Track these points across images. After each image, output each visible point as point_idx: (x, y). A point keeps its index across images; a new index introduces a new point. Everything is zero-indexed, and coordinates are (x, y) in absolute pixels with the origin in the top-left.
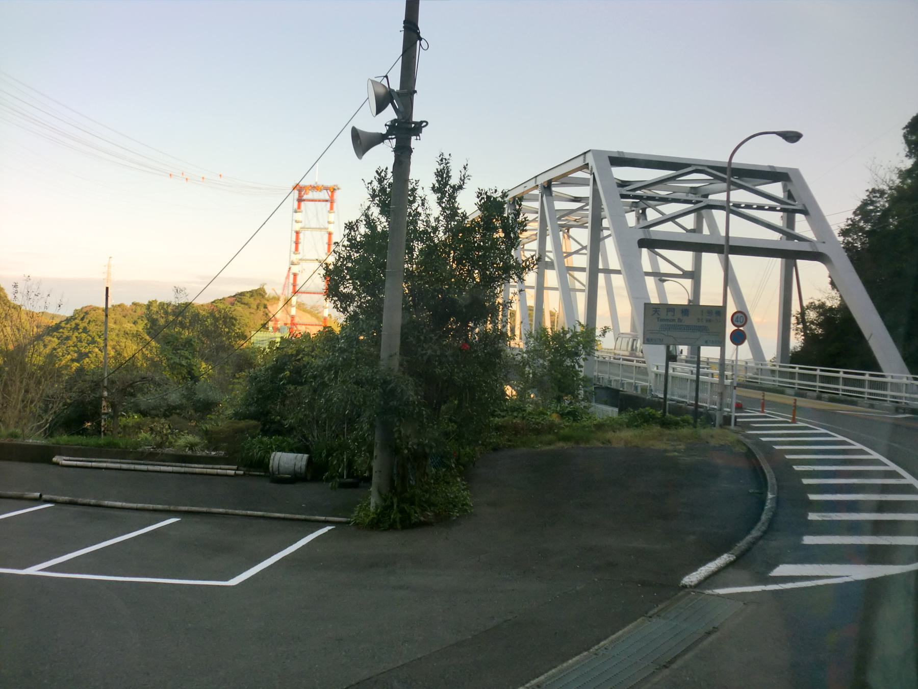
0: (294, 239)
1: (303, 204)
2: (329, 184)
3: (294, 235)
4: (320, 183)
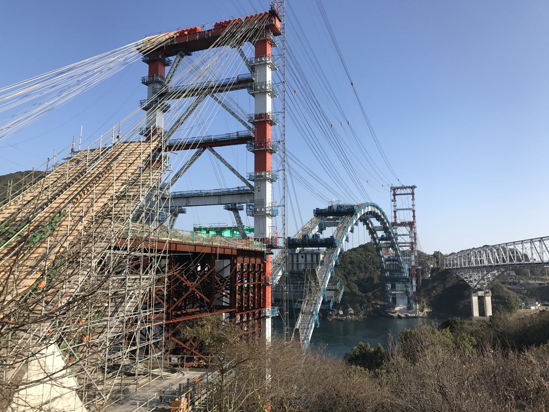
0: (393, 215)
2: (411, 185)
4: (405, 185)
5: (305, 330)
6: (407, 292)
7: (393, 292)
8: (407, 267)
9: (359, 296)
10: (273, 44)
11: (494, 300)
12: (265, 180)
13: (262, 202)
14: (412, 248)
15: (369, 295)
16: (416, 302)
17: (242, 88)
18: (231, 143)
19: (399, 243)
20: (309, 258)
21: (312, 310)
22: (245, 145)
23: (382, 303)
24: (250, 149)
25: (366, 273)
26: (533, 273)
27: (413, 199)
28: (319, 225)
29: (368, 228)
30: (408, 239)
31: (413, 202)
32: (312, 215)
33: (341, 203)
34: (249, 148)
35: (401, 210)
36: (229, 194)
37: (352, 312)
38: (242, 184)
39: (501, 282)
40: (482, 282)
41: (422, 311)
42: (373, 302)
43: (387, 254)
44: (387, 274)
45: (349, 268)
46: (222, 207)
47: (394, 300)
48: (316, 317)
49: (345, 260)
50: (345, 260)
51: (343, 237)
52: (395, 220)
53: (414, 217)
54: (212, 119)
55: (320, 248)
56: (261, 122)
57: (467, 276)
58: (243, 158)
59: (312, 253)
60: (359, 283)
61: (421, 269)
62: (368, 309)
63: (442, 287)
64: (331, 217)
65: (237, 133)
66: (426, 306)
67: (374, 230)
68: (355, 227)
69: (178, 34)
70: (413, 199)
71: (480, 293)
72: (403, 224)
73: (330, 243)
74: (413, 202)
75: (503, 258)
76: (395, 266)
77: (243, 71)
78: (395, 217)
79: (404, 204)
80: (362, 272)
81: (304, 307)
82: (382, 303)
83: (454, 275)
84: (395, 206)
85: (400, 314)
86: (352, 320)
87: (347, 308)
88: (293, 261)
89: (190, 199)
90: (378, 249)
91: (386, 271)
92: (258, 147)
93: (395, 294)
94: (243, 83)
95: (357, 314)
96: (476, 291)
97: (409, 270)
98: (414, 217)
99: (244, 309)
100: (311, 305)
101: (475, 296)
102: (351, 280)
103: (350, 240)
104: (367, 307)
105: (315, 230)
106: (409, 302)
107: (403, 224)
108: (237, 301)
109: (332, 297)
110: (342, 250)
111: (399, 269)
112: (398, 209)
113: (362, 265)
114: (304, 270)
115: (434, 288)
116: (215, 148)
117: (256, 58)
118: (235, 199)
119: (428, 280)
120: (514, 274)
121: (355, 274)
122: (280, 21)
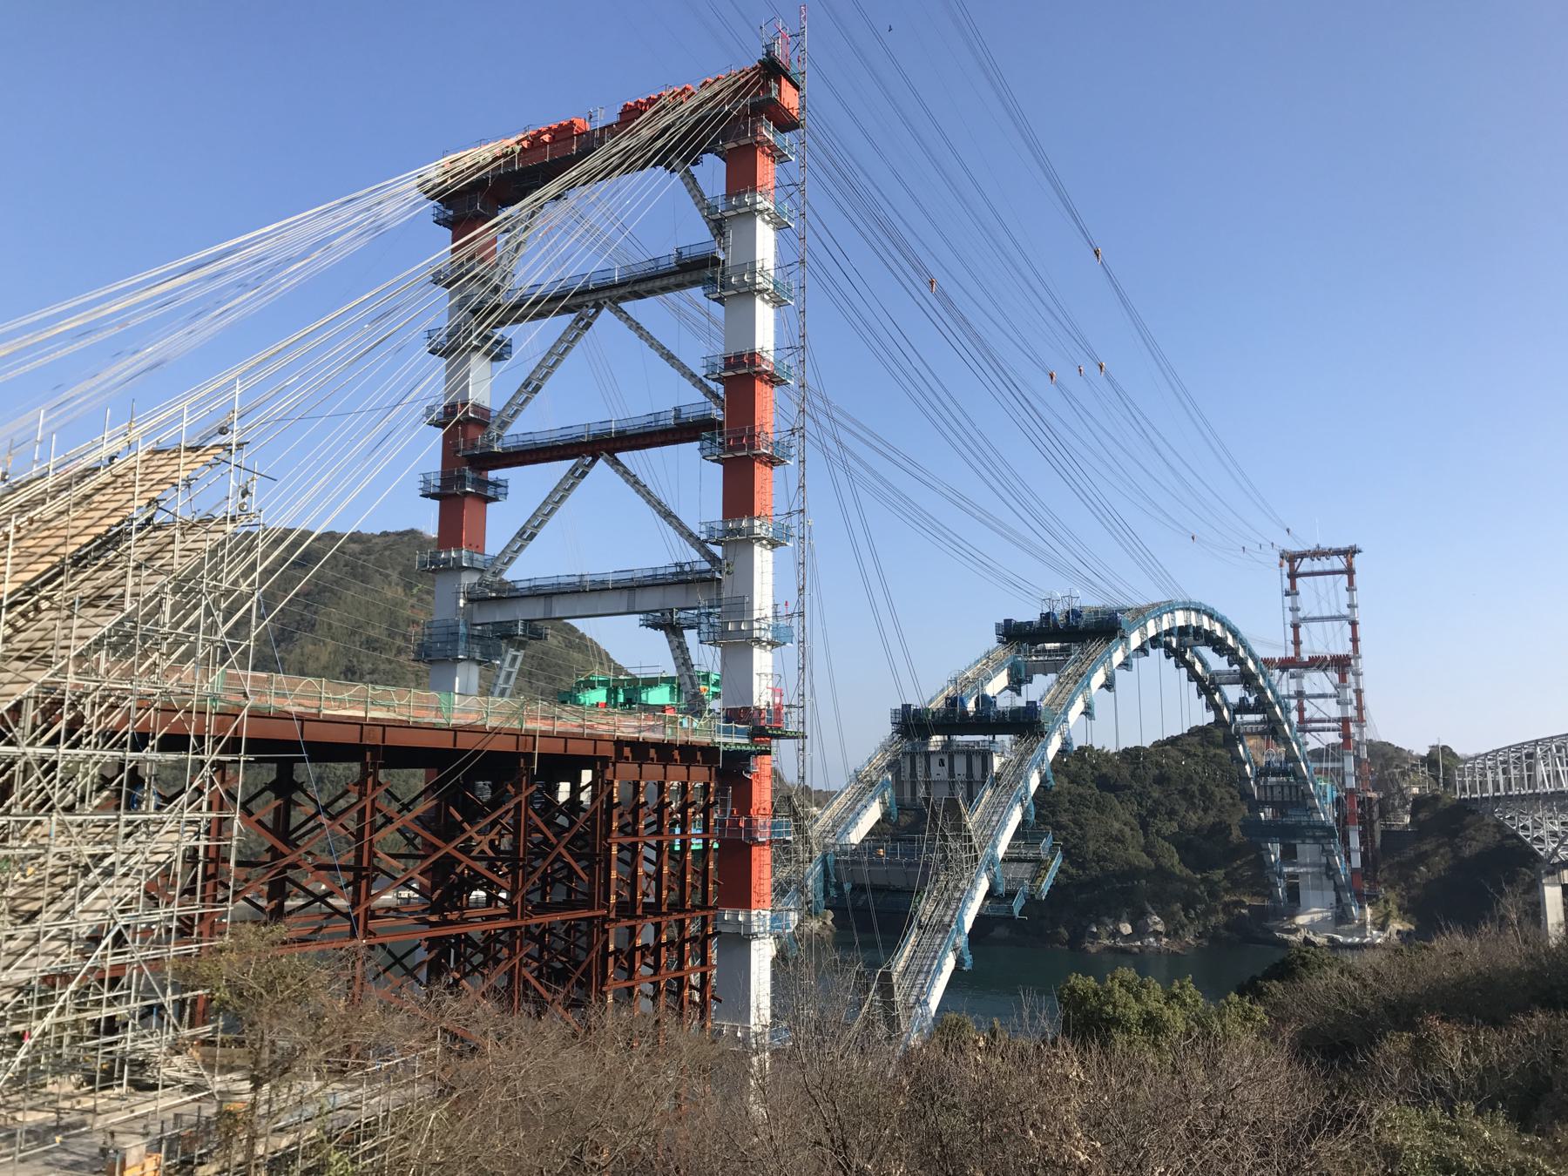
0: (1290, 636)
2: (1344, 545)
4: (1325, 545)
5: (922, 976)
6: (1330, 871)
7: (1286, 870)
8: (1331, 793)
10: (778, 156)
12: (749, 540)
13: (742, 606)
15: (1215, 878)
16: (1361, 898)
18: (670, 437)
19: (1311, 721)
20: (960, 765)
21: (947, 919)
22: (697, 444)
23: (1256, 902)
24: (712, 454)
25: (1205, 810)
27: (1351, 587)
28: (1010, 669)
29: (1193, 676)
30: (1332, 709)
31: (1352, 598)
32: (991, 641)
33: (1076, 605)
34: (707, 452)
35: (1314, 619)
36: (654, 582)
37: (1160, 928)
41: (1383, 928)
42: (1227, 898)
43: (1253, 752)
44: (1265, 814)
45: (1156, 795)
46: (635, 619)
47: (1293, 893)
48: (962, 941)
49: (1140, 772)
50: (1140, 772)
51: (1072, 702)
54: (618, 374)
55: (998, 738)
56: (741, 376)
57: (1529, 823)
58: (691, 479)
59: (969, 753)
60: (1185, 845)
61: (1379, 801)
62: (1213, 920)
63: (1450, 855)
64: (1049, 646)
66: (1395, 913)
67: (1212, 681)
68: (1121, 675)
69: (525, 144)
70: (1351, 587)
72: (1317, 663)
73: (1027, 724)
74: (1352, 598)
76: (1286, 791)
77: (695, 235)
78: (1297, 642)
79: (1324, 605)
80: (1192, 806)
81: (926, 908)
83: (1488, 819)
84: (1294, 609)
85: (1311, 936)
88: (913, 774)
89: (554, 598)
91: (1262, 804)
92: (731, 449)
93: (1294, 876)
94: (695, 270)
95: (1176, 932)
97: (1338, 803)
99: (639, 912)
100: (947, 905)
101: (1553, 884)
102: (1158, 832)
106: (1339, 900)
107: (1317, 663)
108: (613, 888)
110: (1066, 743)
111: (1299, 798)
112: (1305, 619)
113: (1195, 788)
115: (1422, 858)
116: (622, 456)
117: (728, 196)
119: (1402, 833)
121: (1171, 814)
122: (797, 87)
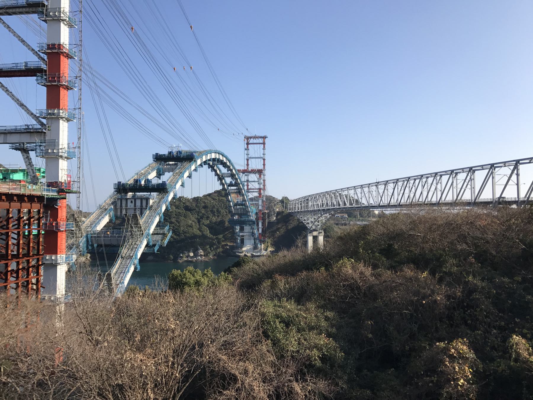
0: (246, 163)
1: (249, 145)
2: (263, 135)
3: (246, 161)
4: (258, 135)
5: (122, 274)
6: (253, 234)
9: (210, 238)
11: (326, 239)
12: (58, 118)
13: (55, 143)
14: (260, 194)
16: (262, 242)
17: (34, 12)
20: (138, 203)
21: (131, 255)
22: (35, 78)
23: (231, 244)
25: (218, 216)
26: (361, 216)
27: (264, 148)
29: (217, 174)
30: (256, 186)
32: (151, 160)
33: (180, 149)
35: (253, 158)
37: (202, 254)
38: (32, 122)
39: (335, 224)
40: (316, 223)
41: (266, 250)
42: (223, 243)
43: (233, 198)
44: (236, 217)
45: (203, 212)
47: (242, 241)
48: (137, 261)
49: (199, 205)
52: (248, 168)
53: (264, 165)
55: (152, 193)
56: (54, 53)
57: (306, 219)
58: (33, 92)
59: (141, 199)
60: (211, 227)
64: (171, 163)
65: (26, 63)
66: (270, 246)
67: (222, 176)
70: (264, 148)
71: (315, 233)
72: (253, 171)
73: (162, 189)
75: (344, 201)
78: (248, 165)
80: (214, 215)
82: (231, 244)
84: (248, 154)
85: (246, 254)
86: (201, 261)
87: (198, 249)
90: (227, 195)
91: (235, 214)
92: (50, 81)
93: (243, 236)
96: (311, 232)
98: (264, 165)
100: (132, 250)
102: (203, 224)
103: (185, 185)
104: (216, 249)
105: (152, 176)
106: (255, 242)
107: (253, 171)
109: (158, 241)
110: (175, 195)
111: (245, 213)
112: (250, 158)
113: (215, 210)
114: (126, 215)
115: (278, 229)
118: (25, 138)
120: (347, 216)
121: (208, 218)
